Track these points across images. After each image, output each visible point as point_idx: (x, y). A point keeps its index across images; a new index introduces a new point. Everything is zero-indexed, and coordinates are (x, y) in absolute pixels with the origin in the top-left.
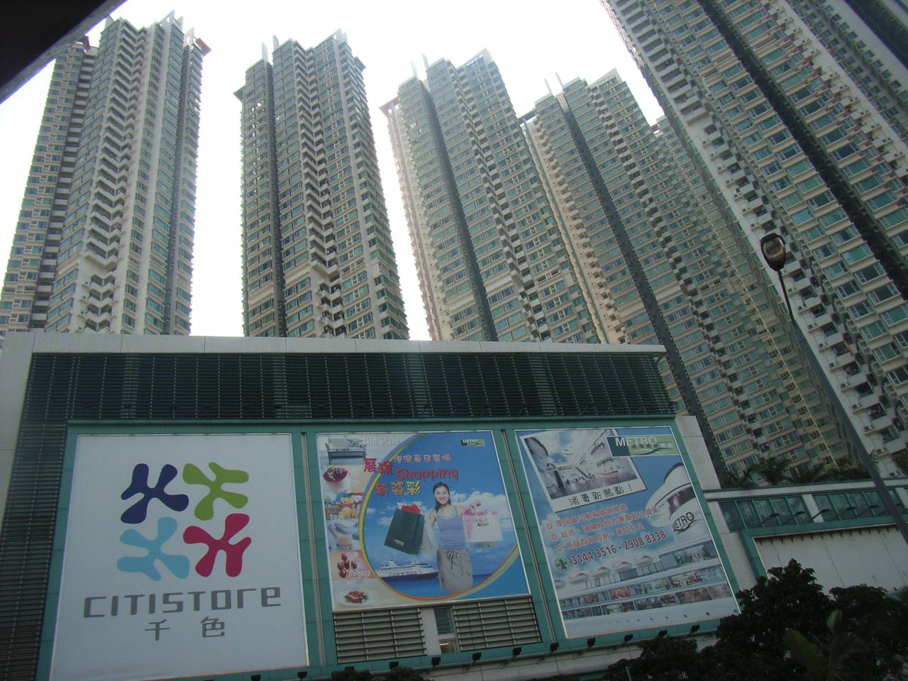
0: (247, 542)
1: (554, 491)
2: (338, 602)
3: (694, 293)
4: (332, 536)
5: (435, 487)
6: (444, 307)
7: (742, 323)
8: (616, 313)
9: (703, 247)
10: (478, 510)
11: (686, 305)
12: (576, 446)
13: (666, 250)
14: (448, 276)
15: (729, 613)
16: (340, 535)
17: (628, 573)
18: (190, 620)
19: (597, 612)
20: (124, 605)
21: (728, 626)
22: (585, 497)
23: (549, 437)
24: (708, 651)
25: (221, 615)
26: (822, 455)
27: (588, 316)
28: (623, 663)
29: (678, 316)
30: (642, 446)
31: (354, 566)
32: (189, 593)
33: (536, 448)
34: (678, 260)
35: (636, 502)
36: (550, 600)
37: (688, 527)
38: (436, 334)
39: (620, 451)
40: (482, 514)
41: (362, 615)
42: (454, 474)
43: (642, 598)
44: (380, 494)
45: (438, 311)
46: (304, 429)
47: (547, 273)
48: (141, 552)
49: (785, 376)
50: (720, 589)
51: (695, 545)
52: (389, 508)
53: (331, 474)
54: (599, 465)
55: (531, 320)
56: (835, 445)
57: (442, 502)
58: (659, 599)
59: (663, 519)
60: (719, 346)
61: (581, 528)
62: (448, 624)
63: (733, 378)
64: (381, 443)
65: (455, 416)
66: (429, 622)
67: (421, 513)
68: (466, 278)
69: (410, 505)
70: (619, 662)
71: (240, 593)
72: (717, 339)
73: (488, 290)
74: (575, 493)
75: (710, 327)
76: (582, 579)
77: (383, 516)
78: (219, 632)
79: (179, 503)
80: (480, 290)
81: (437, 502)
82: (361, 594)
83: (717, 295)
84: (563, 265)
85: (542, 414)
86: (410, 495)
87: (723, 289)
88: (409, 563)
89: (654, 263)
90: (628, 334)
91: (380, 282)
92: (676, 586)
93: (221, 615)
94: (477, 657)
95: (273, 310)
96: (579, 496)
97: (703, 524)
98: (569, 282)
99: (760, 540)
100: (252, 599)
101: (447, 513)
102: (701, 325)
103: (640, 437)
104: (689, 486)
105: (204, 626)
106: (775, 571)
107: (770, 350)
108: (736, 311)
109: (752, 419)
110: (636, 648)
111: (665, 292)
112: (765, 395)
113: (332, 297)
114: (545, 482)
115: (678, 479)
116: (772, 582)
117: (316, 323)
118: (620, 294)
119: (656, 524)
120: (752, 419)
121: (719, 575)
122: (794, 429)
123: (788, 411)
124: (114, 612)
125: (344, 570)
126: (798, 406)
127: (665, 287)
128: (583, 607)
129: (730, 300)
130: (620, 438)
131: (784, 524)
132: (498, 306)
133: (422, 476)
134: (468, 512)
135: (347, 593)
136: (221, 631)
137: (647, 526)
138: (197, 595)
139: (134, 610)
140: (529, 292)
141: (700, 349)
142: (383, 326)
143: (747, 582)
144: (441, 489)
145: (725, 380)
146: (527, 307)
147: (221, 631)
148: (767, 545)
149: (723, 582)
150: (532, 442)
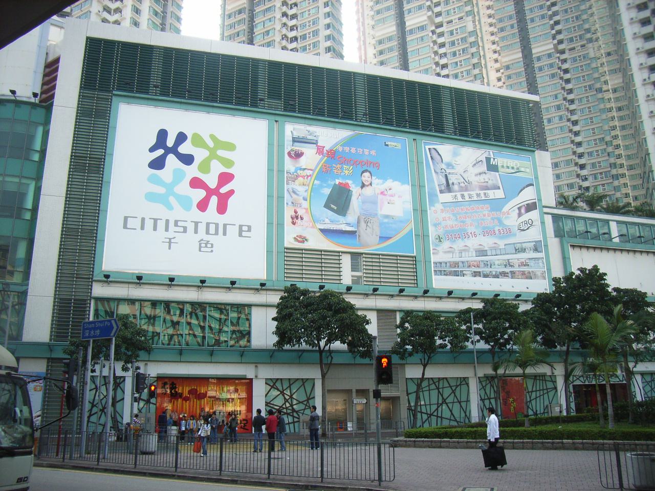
0: (231, 192)
1: (443, 188)
2: (289, 241)
3: (563, 52)
4: (290, 197)
5: (363, 172)
6: (372, 32)
7: (593, 82)
8: (499, 58)
9: (580, 15)
10: (389, 192)
11: (555, 60)
12: (462, 158)
13: (550, 13)
14: (379, 8)
15: (541, 291)
16: (294, 196)
17: (482, 253)
18: (190, 240)
19: (456, 274)
20: (149, 224)
21: (541, 300)
22: (463, 196)
23: (446, 149)
24: (525, 313)
25: (211, 238)
26: (624, 191)
27: (479, 57)
28: (469, 311)
29: (546, 68)
30: (508, 167)
31: (302, 219)
33: (435, 156)
34: (557, 23)
35: (497, 205)
36: (427, 261)
37: (528, 229)
38: (363, 52)
39: (492, 168)
40: (392, 196)
41: (304, 252)
42: (377, 165)
43: (487, 270)
44: (325, 172)
45: (367, 34)
46: (277, 118)
47: (454, 18)
48: (161, 190)
49: (614, 128)
50: (539, 274)
51: (530, 242)
52: (329, 182)
53: (292, 153)
54: (476, 175)
55: (436, 53)
56: (636, 185)
57: (366, 183)
58: (498, 273)
59: (512, 221)
60: (570, 97)
62: (358, 266)
63: (575, 123)
64: (330, 135)
65: (384, 124)
66: (346, 261)
67: (351, 189)
68: (392, 12)
69: (344, 182)
70: (467, 309)
71: (225, 226)
72: (570, 91)
73: (407, 24)
74: (456, 192)
75: (568, 81)
76: (451, 251)
77: (326, 187)
78: (210, 250)
79: (187, 160)
80: (401, 24)
81: (363, 183)
82: (304, 238)
83: (580, 56)
84: (468, 14)
85: (443, 133)
86: (344, 175)
87: (587, 52)
88: (339, 221)
89: (538, 22)
90: (505, 76)
91: (328, 6)
92: (511, 266)
93: (211, 238)
94: (375, 290)
95: (245, 16)
96: (459, 194)
97: (539, 228)
98: (470, 28)
99: (573, 246)
100: (233, 231)
101: (368, 191)
102: (561, 78)
103: (509, 160)
104: (534, 201)
105: (200, 244)
106: (582, 270)
107: (608, 106)
108: (591, 72)
109: (581, 156)
110: (479, 301)
111: (541, 47)
112: (595, 140)
113: (290, 12)
114: (438, 180)
115: (528, 195)
116: (578, 277)
117: (276, 31)
118: (506, 43)
119: (507, 222)
120: (581, 156)
121: (541, 264)
122: (609, 169)
123: (609, 155)
124: (142, 228)
125: (295, 220)
126: (617, 152)
127: (542, 43)
128: (448, 269)
129: (589, 62)
130: (494, 159)
131: (592, 239)
132: (412, 38)
133: (355, 163)
134: (382, 193)
135: (295, 236)
136: (210, 249)
137: (500, 222)
138: (196, 224)
139: (155, 229)
140: (439, 30)
141: (556, 97)
142: (326, 41)
143: (559, 273)
144: (367, 174)
145: (569, 124)
146: (435, 42)
147: (210, 249)
148: (577, 250)
149: (542, 270)
150: (433, 152)
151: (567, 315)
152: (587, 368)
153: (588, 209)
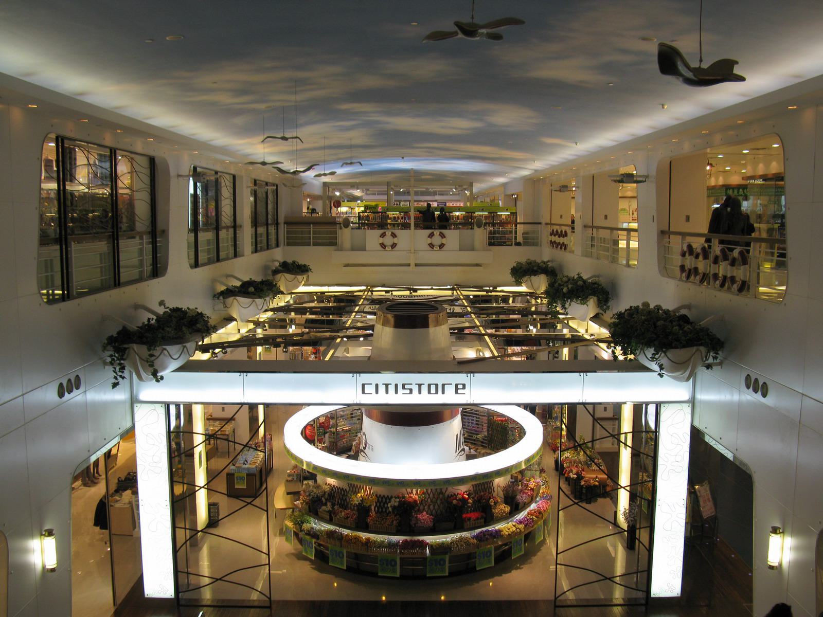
32: (416, 384)
61: (606, 309)
71: (443, 385)
124: (377, 392)
138: (420, 386)
139: (387, 392)
151: (399, 528)
152: (197, 347)
153: (74, 192)
